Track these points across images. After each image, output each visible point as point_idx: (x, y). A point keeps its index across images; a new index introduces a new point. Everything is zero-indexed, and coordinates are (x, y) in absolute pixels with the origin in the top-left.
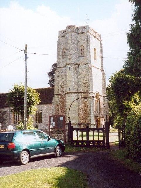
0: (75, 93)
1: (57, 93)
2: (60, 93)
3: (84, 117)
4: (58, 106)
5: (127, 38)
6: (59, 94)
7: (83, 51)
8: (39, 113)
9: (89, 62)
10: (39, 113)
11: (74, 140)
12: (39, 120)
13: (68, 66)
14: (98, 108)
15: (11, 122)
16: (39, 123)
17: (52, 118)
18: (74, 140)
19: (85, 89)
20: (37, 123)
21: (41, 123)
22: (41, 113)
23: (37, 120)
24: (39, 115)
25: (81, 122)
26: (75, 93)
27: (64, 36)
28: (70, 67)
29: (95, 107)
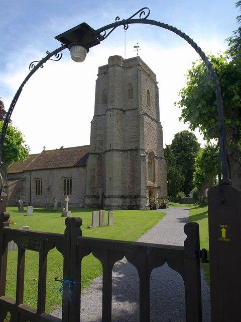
0: (117, 150)
1: (94, 152)
2: (98, 151)
3: (131, 186)
4: (94, 170)
5: (160, 121)
6: (96, 154)
7: (132, 92)
8: (68, 180)
9: (140, 107)
10: (68, 180)
11: (88, 143)
12: (68, 191)
13: (109, 113)
14: (152, 174)
15: (32, 192)
16: (39, 194)
17: (223, 237)
18: (88, 143)
19: (133, 146)
20: (37, 194)
21: (41, 194)
22: (71, 181)
23: (65, 190)
24: (68, 183)
25: (126, 195)
26: (117, 150)
27: (105, 73)
28: (111, 113)
29: (147, 172)
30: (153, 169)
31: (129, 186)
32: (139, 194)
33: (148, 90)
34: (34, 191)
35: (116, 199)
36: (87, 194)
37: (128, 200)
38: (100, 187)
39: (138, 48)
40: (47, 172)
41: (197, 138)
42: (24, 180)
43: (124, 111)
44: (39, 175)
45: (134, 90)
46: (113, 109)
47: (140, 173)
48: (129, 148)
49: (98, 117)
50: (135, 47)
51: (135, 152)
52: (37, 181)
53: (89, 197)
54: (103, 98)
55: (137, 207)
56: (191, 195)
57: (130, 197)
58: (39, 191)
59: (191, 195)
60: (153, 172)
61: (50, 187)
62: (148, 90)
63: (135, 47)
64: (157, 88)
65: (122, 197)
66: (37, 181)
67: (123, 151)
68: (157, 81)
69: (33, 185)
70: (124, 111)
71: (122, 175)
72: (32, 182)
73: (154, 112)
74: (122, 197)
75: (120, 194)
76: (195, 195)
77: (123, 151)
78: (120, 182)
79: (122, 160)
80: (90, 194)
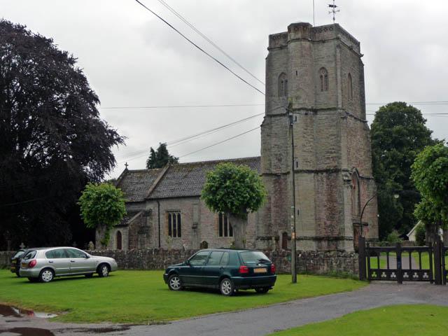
0: (309, 172)
2: (274, 171)
3: (328, 223)
15: (162, 233)
19: (332, 164)
22: (179, 216)
25: (323, 234)
26: (309, 172)
30: (357, 197)
31: (325, 223)
32: (341, 235)
33: (349, 74)
34: (165, 230)
35: (309, 242)
36: (261, 235)
37: (324, 244)
38: (280, 225)
39: (336, 9)
40: (188, 202)
41: (424, 117)
42: (148, 213)
43: (315, 111)
44: (174, 205)
45: (330, 79)
46: (299, 109)
47: (343, 204)
48: (324, 167)
49: (273, 118)
50: (330, 6)
51: (334, 174)
52: (170, 216)
53: (263, 239)
54: (374, 161)
55: (218, 292)
56: (412, 237)
57: (328, 239)
58: (175, 230)
59: (412, 237)
60: (357, 201)
61: (197, 224)
62: (349, 74)
63: (330, 6)
64: (361, 65)
65: (318, 239)
66: (170, 216)
67: (317, 172)
68: (362, 52)
69: (164, 221)
70: (315, 111)
71: (315, 207)
72: (161, 216)
73: (359, 110)
74: (318, 239)
75: (312, 234)
76: (420, 237)
77: (317, 172)
78: (313, 217)
79: (315, 185)
80: (264, 235)
